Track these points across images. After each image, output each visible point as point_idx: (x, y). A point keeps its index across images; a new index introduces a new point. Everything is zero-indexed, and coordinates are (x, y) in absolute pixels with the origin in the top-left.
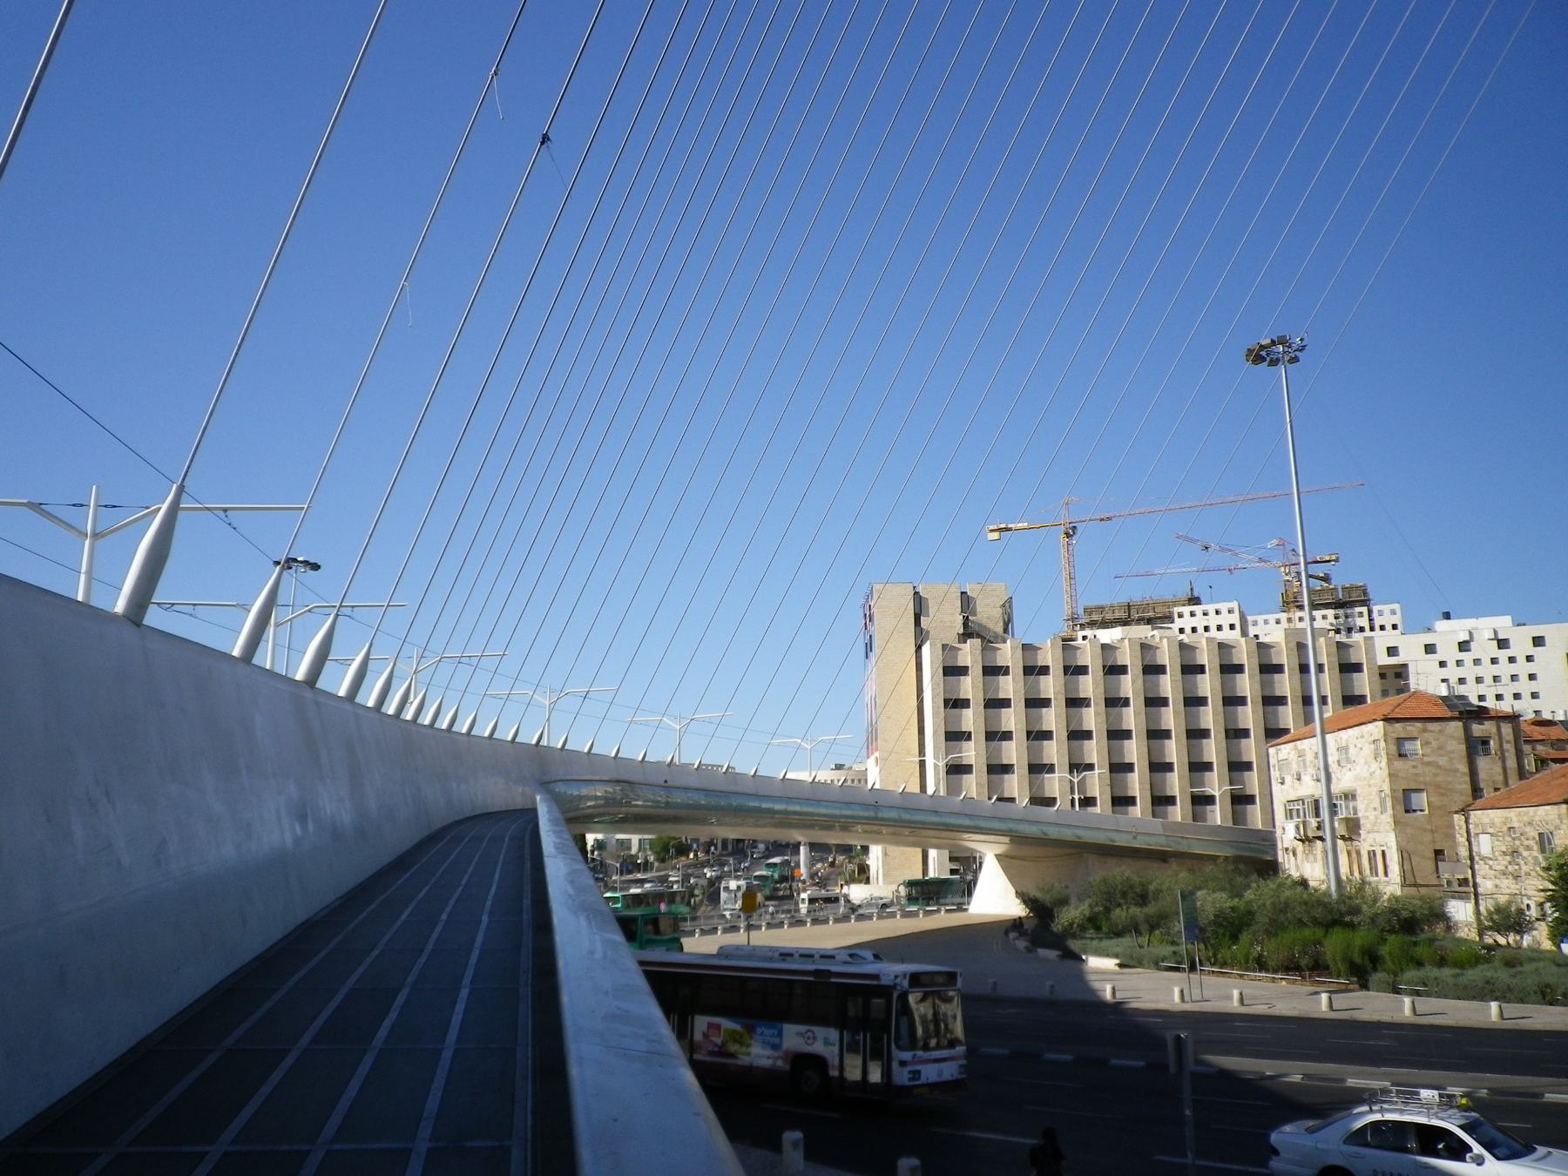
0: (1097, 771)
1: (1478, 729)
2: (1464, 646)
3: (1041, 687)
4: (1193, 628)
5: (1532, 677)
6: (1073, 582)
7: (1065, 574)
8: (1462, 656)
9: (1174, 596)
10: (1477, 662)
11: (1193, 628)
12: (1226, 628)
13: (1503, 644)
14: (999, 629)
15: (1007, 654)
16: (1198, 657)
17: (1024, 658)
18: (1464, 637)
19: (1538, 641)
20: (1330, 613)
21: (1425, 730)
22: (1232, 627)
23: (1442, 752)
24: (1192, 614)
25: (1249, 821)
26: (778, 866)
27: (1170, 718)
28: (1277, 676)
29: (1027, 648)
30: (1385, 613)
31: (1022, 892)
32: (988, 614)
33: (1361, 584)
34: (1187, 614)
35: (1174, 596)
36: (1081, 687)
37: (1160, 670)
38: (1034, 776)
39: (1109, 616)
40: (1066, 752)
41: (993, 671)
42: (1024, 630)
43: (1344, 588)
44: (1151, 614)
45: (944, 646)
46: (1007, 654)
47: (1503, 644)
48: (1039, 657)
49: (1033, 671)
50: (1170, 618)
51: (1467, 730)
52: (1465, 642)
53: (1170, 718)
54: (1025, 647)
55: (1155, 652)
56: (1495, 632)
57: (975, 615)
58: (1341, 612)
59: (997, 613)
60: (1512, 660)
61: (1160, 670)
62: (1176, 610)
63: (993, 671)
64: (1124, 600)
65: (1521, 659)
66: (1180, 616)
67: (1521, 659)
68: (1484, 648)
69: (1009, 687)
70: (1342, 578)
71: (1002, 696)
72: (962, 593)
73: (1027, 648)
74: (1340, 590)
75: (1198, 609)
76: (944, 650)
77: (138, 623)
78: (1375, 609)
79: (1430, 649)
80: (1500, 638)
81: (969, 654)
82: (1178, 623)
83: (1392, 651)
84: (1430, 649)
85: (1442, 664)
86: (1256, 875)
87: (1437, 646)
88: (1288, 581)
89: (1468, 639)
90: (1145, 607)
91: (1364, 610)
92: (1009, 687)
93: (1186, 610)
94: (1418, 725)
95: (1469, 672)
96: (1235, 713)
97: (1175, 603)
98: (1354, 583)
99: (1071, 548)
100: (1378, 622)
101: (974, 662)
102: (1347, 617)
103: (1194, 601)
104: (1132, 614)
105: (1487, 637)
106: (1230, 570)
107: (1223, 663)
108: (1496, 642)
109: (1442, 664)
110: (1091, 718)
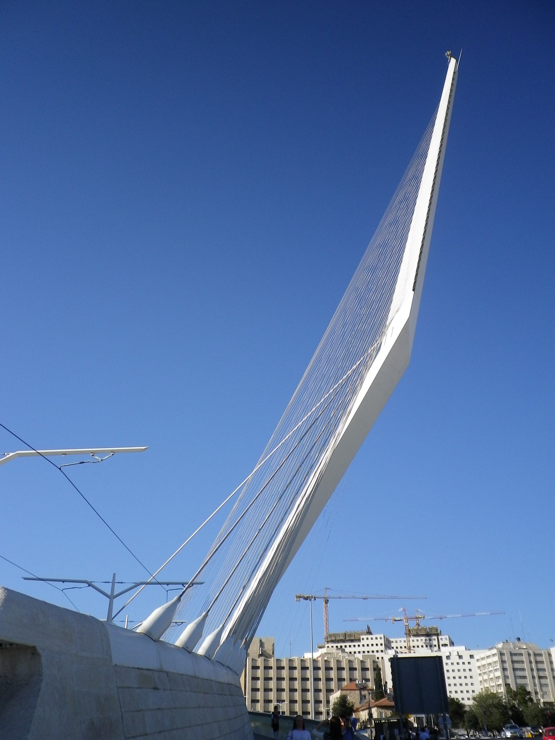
0: (286, 703)
1: (364, 693)
3: (282, 674)
5: (470, 670)
6: (327, 622)
7: (325, 619)
9: (362, 631)
10: (452, 664)
12: (379, 645)
13: (460, 657)
14: (271, 653)
15: (272, 662)
16: (331, 665)
18: (448, 654)
19: (472, 657)
20: (424, 638)
21: (351, 693)
22: (381, 644)
23: (354, 699)
24: (367, 639)
25: (320, 718)
27: (310, 685)
28: (355, 672)
29: (278, 661)
30: (444, 639)
32: (268, 648)
33: (436, 627)
34: (365, 639)
35: (362, 631)
36: (294, 674)
37: (319, 668)
39: (338, 638)
40: (504, 681)
41: (267, 668)
42: (277, 656)
43: (429, 628)
44: (353, 638)
45: (252, 659)
46: (272, 662)
47: (460, 657)
48: (282, 664)
49: (280, 668)
50: (359, 640)
51: (360, 693)
52: (448, 656)
53: (310, 685)
54: (277, 660)
55: (317, 662)
56: (458, 652)
57: (264, 648)
58: (428, 638)
59: (271, 648)
60: (452, 664)
61: (319, 668)
62: (362, 637)
63: (267, 668)
64: (343, 632)
66: (363, 639)
67: (467, 663)
69: (272, 673)
70: (426, 624)
71: (270, 676)
72: (260, 641)
73: (278, 661)
74: (428, 629)
75: (369, 637)
76: (252, 660)
78: (440, 637)
80: (460, 655)
81: (260, 662)
82: (362, 642)
88: (407, 625)
89: (449, 655)
90: (350, 635)
91: (436, 638)
92: (272, 673)
93: (365, 637)
94: (349, 691)
96: (514, 665)
97: (362, 634)
98: (433, 627)
99: (327, 608)
100: (441, 642)
102: (430, 640)
103: (369, 633)
104: (346, 637)
105: (455, 655)
106: (385, 620)
107: (291, 677)
108: (458, 656)
110: (285, 684)
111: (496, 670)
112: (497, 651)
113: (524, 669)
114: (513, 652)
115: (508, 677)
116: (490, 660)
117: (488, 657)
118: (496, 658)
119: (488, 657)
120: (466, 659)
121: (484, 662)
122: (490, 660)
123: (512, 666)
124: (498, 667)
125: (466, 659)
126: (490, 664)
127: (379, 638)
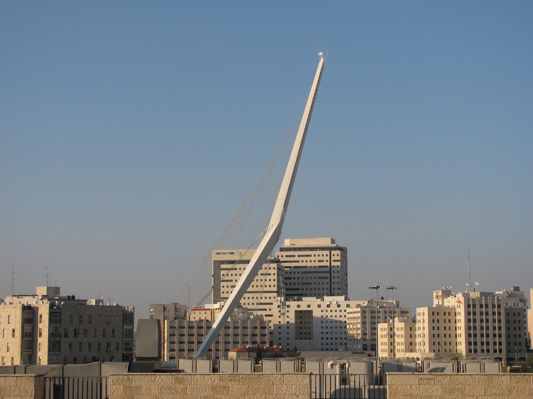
2: (328, 306)
4: (335, 316)
8: (328, 309)
11: (335, 316)
13: (339, 306)
17: (118, 361)
18: (328, 303)
19: (348, 306)
26: (43, 301)
31: (118, 305)
38: (469, 323)
47: (339, 306)
65: (343, 311)
67: (343, 311)
68: (334, 307)
77: (47, 296)
79: (319, 306)
83: (309, 306)
84: (319, 306)
85: (322, 311)
86: (47, 300)
87: (60, 288)
89: (329, 304)
95: (338, 314)
101: (250, 340)
108: (337, 305)
109: (322, 311)
111: (358, 323)
112: (361, 310)
113: (60, 334)
114: (4, 358)
115: (366, 334)
116: (355, 315)
117: (355, 312)
118: (359, 315)
119: (355, 312)
120: (343, 307)
121: (351, 315)
122: (355, 315)
123: (480, 325)
124: (360, 321)
125: (343, 307)
126: (355, 318)
127: (325, 283)
